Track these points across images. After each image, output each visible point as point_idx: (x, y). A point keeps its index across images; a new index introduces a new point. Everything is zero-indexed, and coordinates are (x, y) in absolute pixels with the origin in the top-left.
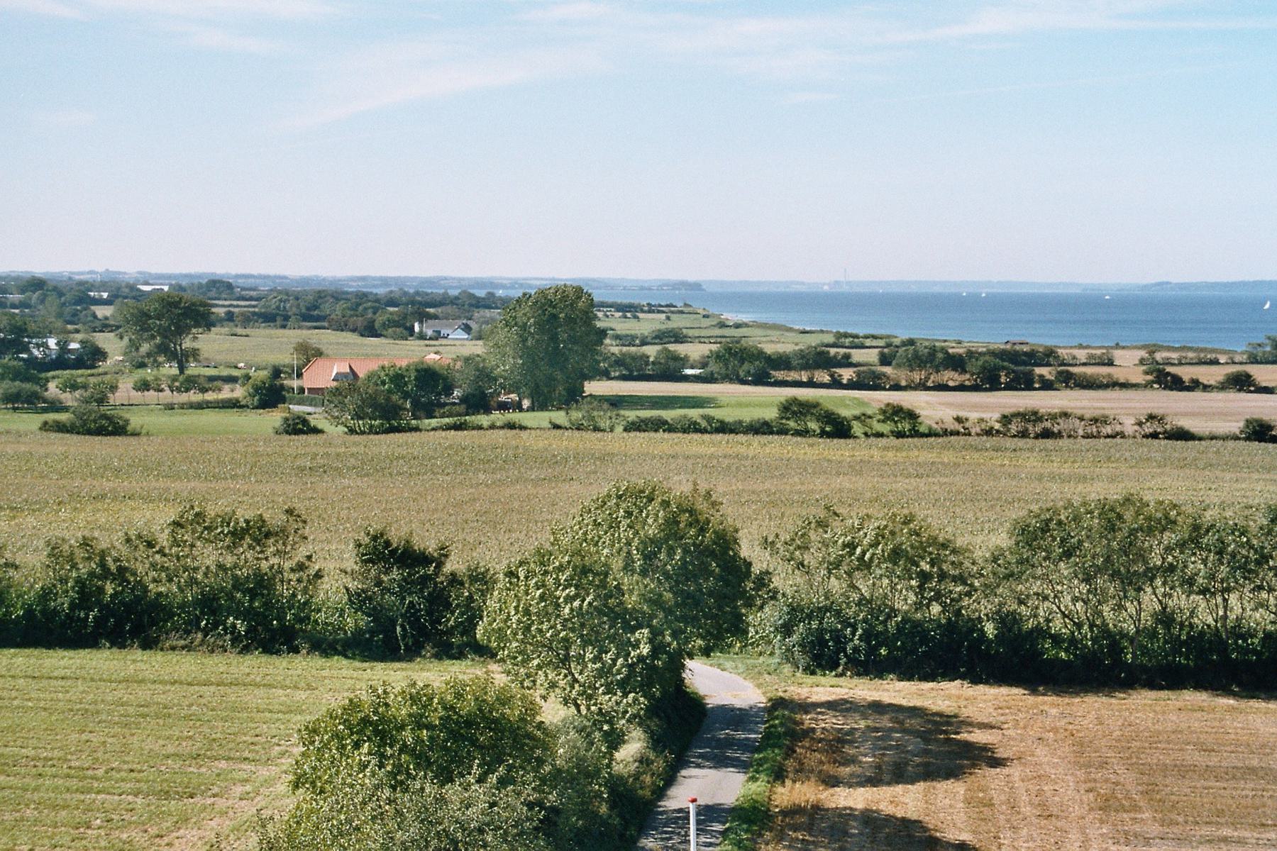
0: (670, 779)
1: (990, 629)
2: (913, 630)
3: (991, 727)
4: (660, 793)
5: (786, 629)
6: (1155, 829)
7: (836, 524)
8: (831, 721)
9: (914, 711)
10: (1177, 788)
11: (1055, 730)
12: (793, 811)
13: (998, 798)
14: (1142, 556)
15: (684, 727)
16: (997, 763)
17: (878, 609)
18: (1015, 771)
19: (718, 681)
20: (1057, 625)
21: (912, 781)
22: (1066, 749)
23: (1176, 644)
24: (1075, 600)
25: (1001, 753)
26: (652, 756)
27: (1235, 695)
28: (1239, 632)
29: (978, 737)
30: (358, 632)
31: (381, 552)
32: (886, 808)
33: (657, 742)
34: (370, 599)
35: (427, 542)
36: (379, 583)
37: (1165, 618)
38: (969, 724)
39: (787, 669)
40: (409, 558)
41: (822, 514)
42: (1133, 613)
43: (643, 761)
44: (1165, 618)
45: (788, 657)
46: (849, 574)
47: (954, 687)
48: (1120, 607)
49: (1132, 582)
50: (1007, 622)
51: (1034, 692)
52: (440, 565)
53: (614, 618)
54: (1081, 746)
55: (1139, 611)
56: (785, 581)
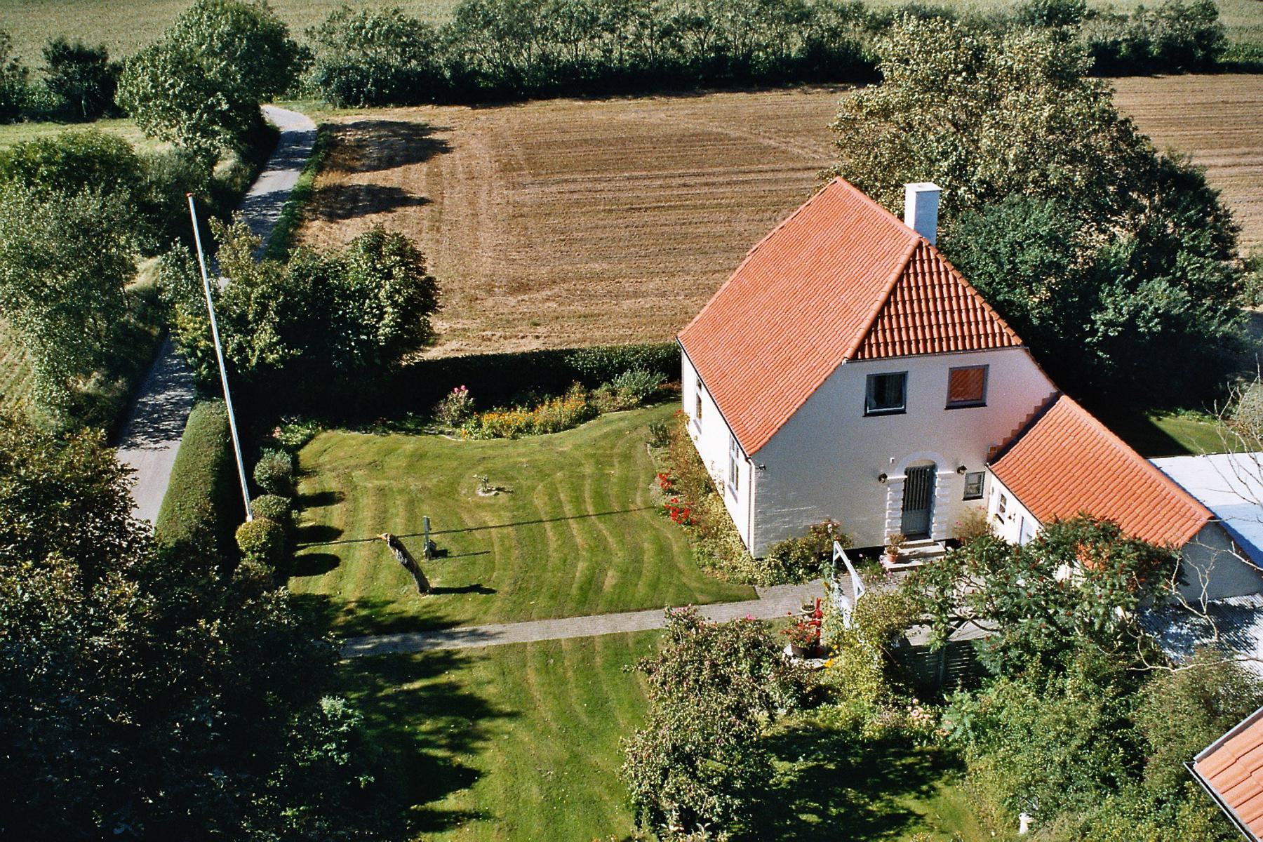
0: (254, 179)
1: (447, 74)
2: (402, 77)
3: (446, 129)
4: (248, 188)
5: (326, 83)
6: (529, 179)
7: (350, 17)
8: (350, 137)
9: (404, 125)
10: (545, 155)
11: (483, 129)
12: (327, 190)
13: (445, 170)
14: (530, 23)
15: (264, 147)
16: (447, 150)
17: (382, 67)
18: (457, 155)
19: (286, 117)
20: (485, 67)
21: (399, 165)
22: (488, 138)
23: (550, 73)
24: (494, 52)
25: (451, 145)
26: (242, 166)
27: (582, 99)
28: (584, 63)
29: (438, 136)
30: (61, 105)
31: (60, 55)
32: (381, 183)
33: (245, 157)
34: (63, 85)
35: (91, 44)
36: (66, 73)
37: (544, 58)
38: (435, 130)
39: (330, 107)
40: (83, 57)
41: (340, 10)
42: (526, 57)
43: (235, 170)
44: (544, 58)
45: (330, 99)
46: (361, 45)
47: (427, 109)
48: (519, 54)
49: (522, 38)
50: (456, 67)
51: (474, 108)
52: (105, 59)
53: (200, 86)
54: (496, 137)
55: (529, 56)
56: (323, 54)
